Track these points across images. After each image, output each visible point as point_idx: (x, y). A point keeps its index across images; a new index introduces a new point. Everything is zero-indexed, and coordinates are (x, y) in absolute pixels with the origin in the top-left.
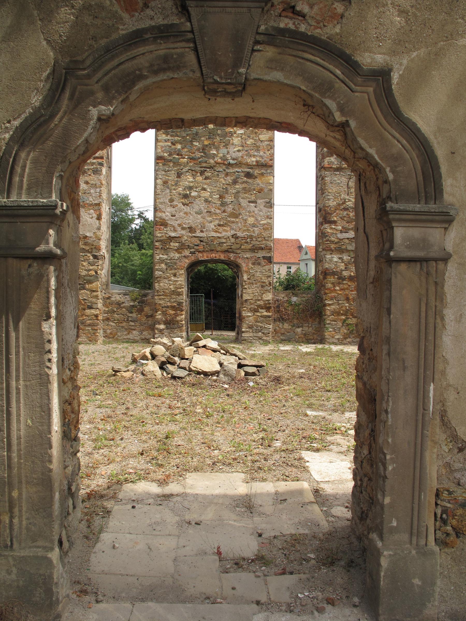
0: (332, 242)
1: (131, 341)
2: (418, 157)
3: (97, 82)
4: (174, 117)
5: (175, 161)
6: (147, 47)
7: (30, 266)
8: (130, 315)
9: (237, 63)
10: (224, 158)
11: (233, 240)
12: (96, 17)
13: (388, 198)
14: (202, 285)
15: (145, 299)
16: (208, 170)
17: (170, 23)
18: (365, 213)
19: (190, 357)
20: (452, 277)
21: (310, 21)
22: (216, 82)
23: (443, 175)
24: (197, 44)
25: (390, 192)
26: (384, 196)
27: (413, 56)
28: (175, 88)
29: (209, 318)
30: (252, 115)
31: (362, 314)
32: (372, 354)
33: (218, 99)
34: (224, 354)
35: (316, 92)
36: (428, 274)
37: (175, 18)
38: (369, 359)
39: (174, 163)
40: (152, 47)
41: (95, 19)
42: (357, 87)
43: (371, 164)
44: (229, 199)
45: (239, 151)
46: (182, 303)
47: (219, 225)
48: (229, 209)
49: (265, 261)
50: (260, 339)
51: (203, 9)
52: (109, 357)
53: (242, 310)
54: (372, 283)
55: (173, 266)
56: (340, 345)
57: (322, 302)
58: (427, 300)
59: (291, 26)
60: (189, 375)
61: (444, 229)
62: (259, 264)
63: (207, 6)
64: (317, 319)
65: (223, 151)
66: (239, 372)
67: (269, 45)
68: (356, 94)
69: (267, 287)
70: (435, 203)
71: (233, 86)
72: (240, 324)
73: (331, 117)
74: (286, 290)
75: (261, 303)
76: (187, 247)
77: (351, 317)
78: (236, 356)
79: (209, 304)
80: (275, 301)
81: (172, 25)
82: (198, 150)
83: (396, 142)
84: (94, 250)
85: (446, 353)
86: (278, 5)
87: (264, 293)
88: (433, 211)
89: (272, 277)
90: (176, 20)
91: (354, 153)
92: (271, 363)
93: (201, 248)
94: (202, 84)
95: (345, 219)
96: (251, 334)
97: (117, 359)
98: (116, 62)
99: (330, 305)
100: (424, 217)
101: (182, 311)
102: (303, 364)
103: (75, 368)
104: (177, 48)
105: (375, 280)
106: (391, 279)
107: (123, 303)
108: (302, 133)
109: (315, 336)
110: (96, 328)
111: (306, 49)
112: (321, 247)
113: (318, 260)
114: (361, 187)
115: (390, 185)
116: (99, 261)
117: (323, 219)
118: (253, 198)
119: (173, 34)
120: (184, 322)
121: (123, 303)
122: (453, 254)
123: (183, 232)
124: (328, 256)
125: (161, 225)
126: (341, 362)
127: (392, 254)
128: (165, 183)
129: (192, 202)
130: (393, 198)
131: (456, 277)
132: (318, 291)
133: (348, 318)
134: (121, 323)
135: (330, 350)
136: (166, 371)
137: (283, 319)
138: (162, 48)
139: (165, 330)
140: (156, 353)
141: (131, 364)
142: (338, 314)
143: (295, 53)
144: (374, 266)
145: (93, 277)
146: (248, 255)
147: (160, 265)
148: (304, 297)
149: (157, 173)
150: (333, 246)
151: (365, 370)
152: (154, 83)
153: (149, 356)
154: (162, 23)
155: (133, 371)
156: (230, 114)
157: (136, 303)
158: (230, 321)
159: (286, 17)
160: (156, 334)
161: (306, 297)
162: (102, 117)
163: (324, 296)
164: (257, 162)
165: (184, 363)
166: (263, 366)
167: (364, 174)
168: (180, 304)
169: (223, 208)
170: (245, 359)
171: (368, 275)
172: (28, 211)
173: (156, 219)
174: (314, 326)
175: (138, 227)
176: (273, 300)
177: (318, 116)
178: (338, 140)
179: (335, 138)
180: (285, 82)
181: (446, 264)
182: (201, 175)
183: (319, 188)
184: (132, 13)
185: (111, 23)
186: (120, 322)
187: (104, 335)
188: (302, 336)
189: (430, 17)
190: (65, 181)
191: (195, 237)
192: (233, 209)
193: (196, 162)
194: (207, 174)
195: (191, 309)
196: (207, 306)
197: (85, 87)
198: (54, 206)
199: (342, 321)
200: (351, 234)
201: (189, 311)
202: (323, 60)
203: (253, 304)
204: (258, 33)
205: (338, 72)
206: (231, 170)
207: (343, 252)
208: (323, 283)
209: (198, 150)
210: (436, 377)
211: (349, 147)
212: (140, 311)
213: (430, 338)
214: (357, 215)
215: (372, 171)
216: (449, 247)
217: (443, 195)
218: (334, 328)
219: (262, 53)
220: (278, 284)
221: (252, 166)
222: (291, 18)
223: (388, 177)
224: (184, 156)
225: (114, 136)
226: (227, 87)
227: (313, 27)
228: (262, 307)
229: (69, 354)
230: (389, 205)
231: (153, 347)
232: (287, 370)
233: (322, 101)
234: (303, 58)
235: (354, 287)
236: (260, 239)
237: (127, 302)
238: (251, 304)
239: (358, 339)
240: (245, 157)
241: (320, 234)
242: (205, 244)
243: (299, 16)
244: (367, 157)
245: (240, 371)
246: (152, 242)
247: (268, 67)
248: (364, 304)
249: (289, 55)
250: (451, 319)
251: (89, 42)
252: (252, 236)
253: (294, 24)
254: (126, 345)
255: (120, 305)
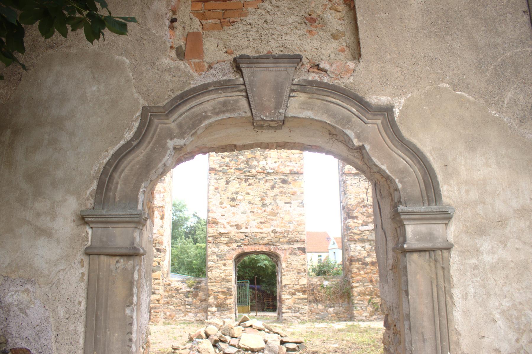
0: (355, 234)
1: (187, 322)
2: (419, 170)
3: (173, 122)
4: (229, 144)
5: (224, 171)
6: (211, 96)
7: (117, 262)
8: (187, 299)
9: (278, 106)
10: (264, 168)
11: (273, 235)
12: (174, 76)
13: (399, 202)
14: (247, 273)
15: (200, 285)
16: (251, 178)
17: (228, 79)
18: (382, 213)
19: (239, 336)
20: (455, 263)
21: (330, 75)
22: (263, 120)
23: (440, 183)
24: (248, 93)
25: (400, 197)
26: (396, 201)
27: (408, 97)
28: (231, 124)
29: (253, 301)
30: (289, 141)
31: (385, 295)
32: (396, 329)
33: (264, 131)
34: (268, 333)
35: (338, 125)
36: (436, 261)
37: (232, 75)
38: (394, 333)
39: (224, 173)
40: (215, 96)
41: (173, 77)
42: (369, 120)
43: (384, 177)
44: (267, 201)
45: (275, 162)
46: (231, 288)
47: (261, 223)
48: (269, 209)
49: (301, 251)
50: (298, 318)
51: (252, 69)
52: (169, 336)
53: (282, 293)
54: (391, 270)
55: (223, 258)
56: (367, 321)
57: (350, 285)
58: (437, 282)
59: (317, 78)
60: (238, 351)
61: (445, 225)
62: (295, 254)
63: (255, 67)
64: (346, 299)
65: (262, 163)
66: (281, 349)
67: (301, 92)
68: (369, 125)
69: (302, 273)
70: (436, 204)
71: (275, 122)
72: (281, 306)
73: (351, 142)
74: (318, 275)
75: (298, 287)
76: (234, 241)
77: (375, 297)
78: (278, 334)
79: (254, 289)
80: (310, 285)
81: (229, 81)
82: (243, 162)
83: (402, 159)
84: (157, 245)
85: (458, 326)
86: (307, 64)
87: (300, 279)
88: (435, 211)
89: (306, 265)
90: (232, 76)
91: (370, 168)
92: (309, 339)
93: (246, 242)
94: (252, 121)
95: (365, 214)
96: (291, 315)
97: (175, 338)
98: (188, 107)
99: (356, 287)
100: (428, 216)
101: (231, 295)
102: (337, 339)
103: (147, 346)
104: (233, 96)
105: (393, 267)
106: (406, 266)
107: (181, 289)
108: (328, 152)
109: (346, 315)
110: (157, 310)
111: (328, 94)
112: (346, 238)
113: (345, 249)
114: (377, 193)
115: (399, 192)
116: (162, 253)
117: (347, 215)
118: (288, 200)
119: (230, 86)
120: (232, 305)
121: (181, 289)
122: (454, 244)
123: (231, 229)
124: (353, 246)
125: (213, 223)
126: (369, 337)
127: (405, 246)
128: (217, 189)
129: (238, 204)
130: (403, 202)
131: (459, 263)
132: (346, 276)
133: (372, 298)
134: (179, 306)
135: (359, 327)
136: (218, 349)
137: (317, 300)
138: (222, 96)
139: (216, 313)
140: (209, 332)
141: (188, 342)
142: (364, 294)
143: (321, 97)
144: (392, 256)
145: (156, 267)
146: (286, 246)
147: (212, 257)
148: (334, 281)
149: (210, 181)
150: (356, 237)
151: (391, 343)
152: (216, 121)
153: (204, 336)
154: (222, 79)
155: (190, 349)
156: (273, 141)
157: (192, 289)
158: (271, 303)
159: (313, 72)
160: (208, 315)
161: (337, 280)
162: (177, 147)
163: (351, 280)
164: (291, 171)
165: (234, 341)
166: (302, 342)
167: (378, 182)
168: (229, 289)
169: (264, 209)
170: (286, 336)
171: (388, 263)
172: (118, 219)
173: (209, 218)
174: (344, 306)
175: (192, 225)
176: (307, 284)
177: (341, 142)
178: (357, 158)
179: (354, 156)
180: (315, 118)
181: (449, 252)
182: (245, 182)
183: (342, 190)
184: (200, 73)
185: (184, 80)
186: (178, 305)
187: (165, 317)
188: (335, 315)
189: (418, 70)
190: (146, 194)
191: (241, 232)
192: (272, 209)
193: (241, 172)
194: (250, 181)
195: (239, 293)
196: (251, 291)
197: (165, 125)
198: (138, 215)
199: (368, 301)
200: (371, 226)
201: (237, 296)
202: (342, 101)
203: (291, 288)
204: (293, 84)
205: (354, 110)
206: (269, 177)
207: (365, 242)
208: (350, 269)
209: (243, 162)
210: (452, 347)
211: (366, 164)
212: (195, 296)
213: (443, 314)
214: (374, 211)
215: (385, 182)
216: (451, 238)
217: (441, 198)
218: (361, 307)
219: (296, 98)
220: (311, 270)
221: (287, 174)
222: (316, 73)
223: (397, 186)
224: (231, 167)
225: (182, 158)
226: (271, 123)
227: (333, 79)
228: (299, 291)
229: (143, 334)
230: (401, 208)
231: (207, 327)
232: (323, 346)
233: (343, 131)
234: (327, 101)
235: (376, 271)
236: (295, 233)
237: (184, 288)
238: (289, 288)
239: (383, 316)
240: (281, 167)
241: (345, 228)
242: (249, 238)
243: (322, 71)
244: (381, 172)
245: (282, 347)
246: (205, 237)
247: (301, 108)
248: (386, 287)
249: (317, 99)
250: (459, 297)
251: (169, 93)
252: (288, 231)
253: (319, 77)
254: (183, 326)
255: (178, 291)
